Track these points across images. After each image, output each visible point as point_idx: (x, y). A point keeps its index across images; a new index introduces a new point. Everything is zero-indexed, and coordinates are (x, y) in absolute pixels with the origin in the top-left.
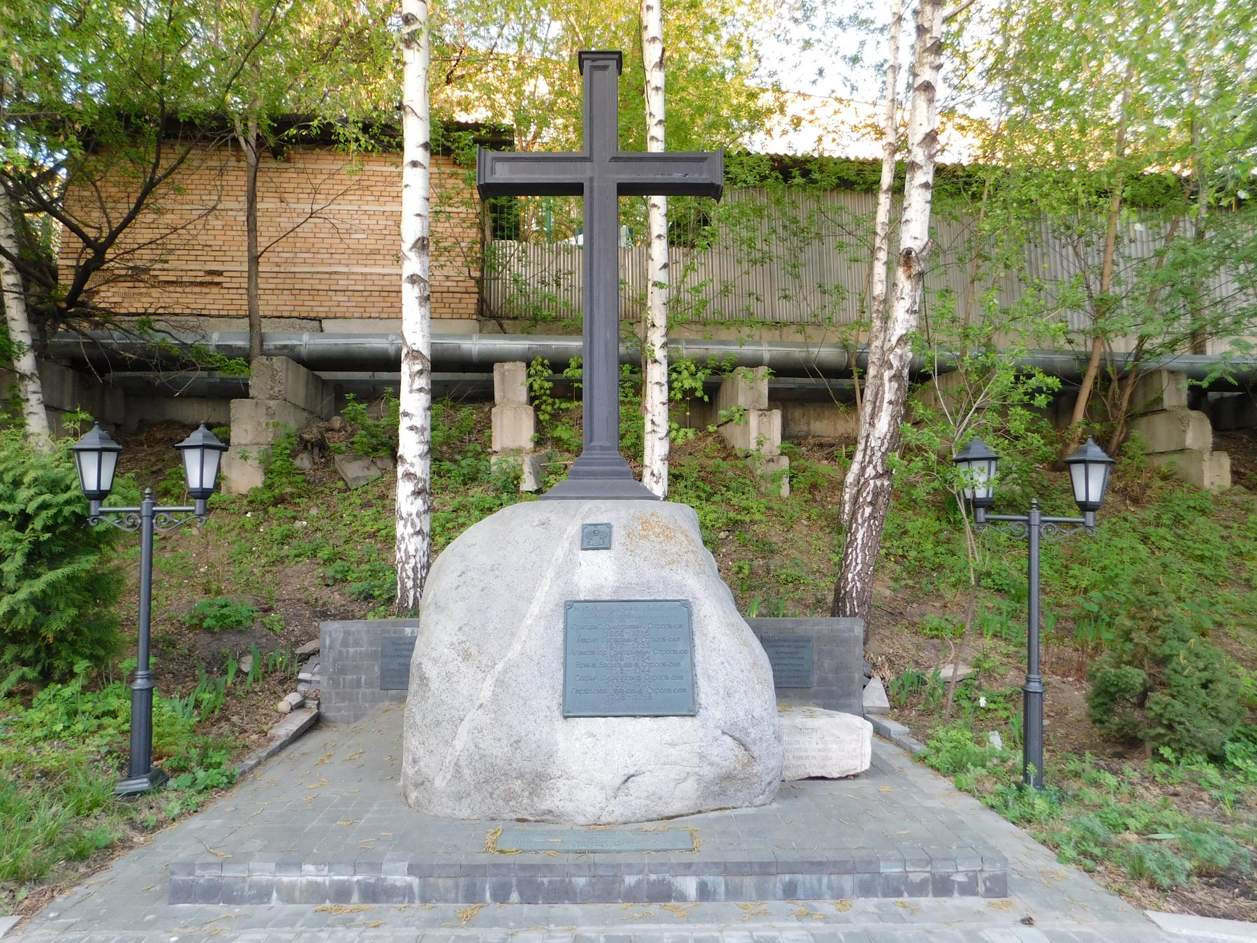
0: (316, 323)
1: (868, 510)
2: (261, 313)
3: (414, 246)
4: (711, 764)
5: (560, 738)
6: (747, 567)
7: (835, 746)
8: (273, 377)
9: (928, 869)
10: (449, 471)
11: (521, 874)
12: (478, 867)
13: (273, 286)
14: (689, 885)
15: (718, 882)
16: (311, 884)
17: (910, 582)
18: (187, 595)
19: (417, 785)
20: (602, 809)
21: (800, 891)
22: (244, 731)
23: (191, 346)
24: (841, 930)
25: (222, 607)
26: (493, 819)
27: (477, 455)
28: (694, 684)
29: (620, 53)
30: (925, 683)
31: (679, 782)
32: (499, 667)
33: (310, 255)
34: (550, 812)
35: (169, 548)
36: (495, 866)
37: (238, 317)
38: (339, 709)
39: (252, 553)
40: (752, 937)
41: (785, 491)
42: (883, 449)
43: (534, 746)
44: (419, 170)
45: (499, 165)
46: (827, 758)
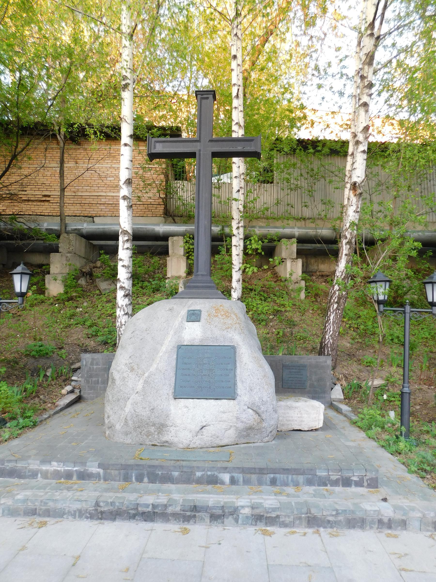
0: (91, 219)
1: (335, 306)
2: (66, 214)
3: (125, 182)
4: (242, 422)
5: (172, 408)
6: (281, 332)
7: (306, 416)
8: (69, 243)
9: (340, 474)
10: (147, 286)
11: (149, 470)
12: (129, 465)
13: (72, 202)
14: (226, 477)
15: (239, 477)
16: (55, 471)
17: (360, 340)
18: (27, 341)
19: (109, 428)
20: (191, 441)
21: (278, 482)
22: (45, 402)
23: (33, 229)
24: (293, 501)
25: (40, 346)
26: (141, 444)
27: (160, 279)
28: (235, 384)
29: (214, 91)
30: (361, 387)
31: (226, 430)
32: (146, 375)
33: (89, 188)
34: (167, 442)
35: (21, 320)
36: (137, 465)
37: (57, 216)
38: (89, 394)
39: (57, 322)
40: (251, 502)
41: (303, 295)
42: (342, 277)
43: (160, 411)
44: (127, 148)
45: (157, 144)
46: (302, 421)
